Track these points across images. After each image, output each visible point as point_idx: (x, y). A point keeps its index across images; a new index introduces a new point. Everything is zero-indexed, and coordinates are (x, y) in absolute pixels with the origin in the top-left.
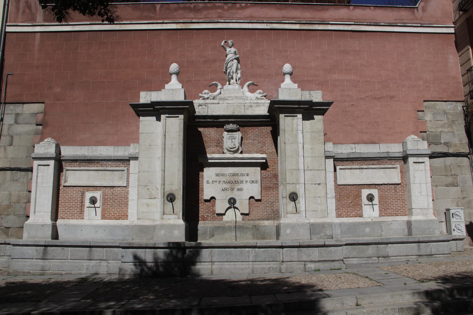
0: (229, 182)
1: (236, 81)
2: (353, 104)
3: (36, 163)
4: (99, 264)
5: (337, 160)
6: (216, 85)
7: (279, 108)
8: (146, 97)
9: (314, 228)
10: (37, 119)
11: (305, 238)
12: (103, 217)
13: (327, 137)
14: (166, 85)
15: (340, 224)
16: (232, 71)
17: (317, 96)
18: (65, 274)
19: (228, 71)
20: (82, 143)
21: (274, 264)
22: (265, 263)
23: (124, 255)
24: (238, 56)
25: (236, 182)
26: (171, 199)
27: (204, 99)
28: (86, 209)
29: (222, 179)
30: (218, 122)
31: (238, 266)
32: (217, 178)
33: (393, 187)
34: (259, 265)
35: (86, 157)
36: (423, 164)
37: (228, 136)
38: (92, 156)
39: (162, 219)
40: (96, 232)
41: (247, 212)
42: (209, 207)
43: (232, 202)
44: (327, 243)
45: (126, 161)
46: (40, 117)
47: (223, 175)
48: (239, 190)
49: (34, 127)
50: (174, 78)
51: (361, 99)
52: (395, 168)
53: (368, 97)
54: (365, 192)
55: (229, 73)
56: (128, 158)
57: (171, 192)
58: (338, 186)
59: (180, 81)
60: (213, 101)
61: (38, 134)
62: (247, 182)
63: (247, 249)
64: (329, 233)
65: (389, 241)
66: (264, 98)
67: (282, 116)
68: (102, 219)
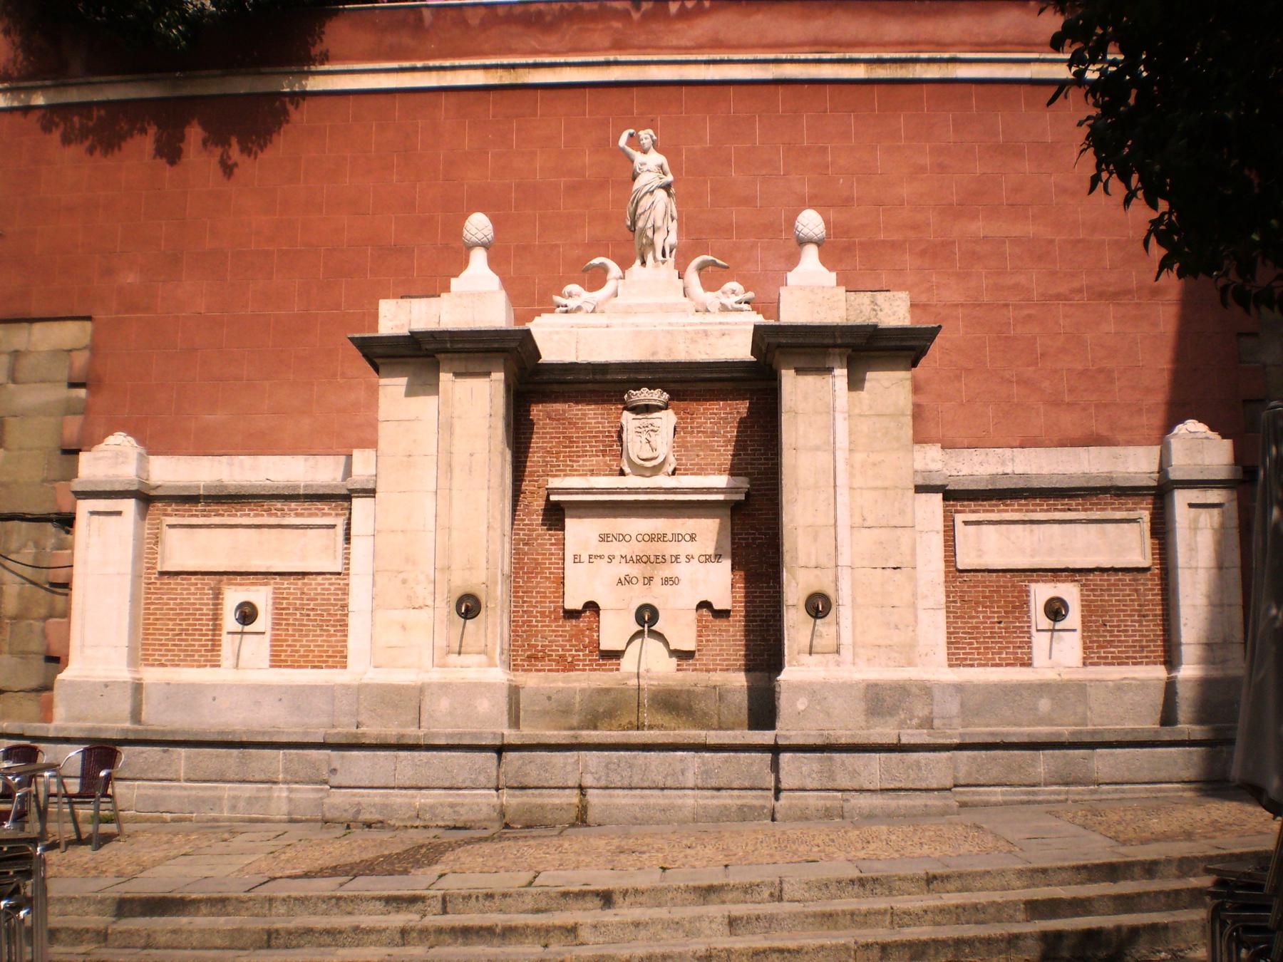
0: (639, 560)
1: (664, 255)
2: (1029, 316)
3: (84, 507)
4: (265, 794)
5: (953, 496)
6: (603, 269)
7: (785, 347)
8: (397, 317)
9: (879, 699)
10: (71, 368)
11: (848, 728)
12: (277, 661)
13: (924, 427)
14: (453, 281)
15: (959, 688)
16: (649, 225)
17: (894, 311)
18: (173, 820)
19: (640, 224)
20: (204, 446)
21: (755, 797)
22: (730, 792)
23: (338, 767)
24: (670, 178)
25: (660, 560)
26: (467, 609)
27: (567, 312)
28: (226, 640)
29: (618, 549)
30: (607, 384)
31: (652, 801)
32: (605, 549)
33: (1128, 577)
34: (713, 797)
35: (226, 487)
36: (1135, 525)
37: (637, 423)
38: (242, 486)
39: (444, 666)
40: (257, 703)
41: (690, 645)
42: (582, 631)
43: (647, 616)
44: (904, 740)
45: (342, 498)
46: (81, 359)
47: (621, 538)
48: (666, 581)
49: (63, 392)
50: (479, 258)
51: (1058, 297)
52: (1134, 521)
53: (1080, 291)
54: (1041, 593)
55: (643, 230)
56: (345, 492)
57: (469, 590)
58: (954, 572)
59: (493, 263)
60: (592, 319)
61: (74, 414)
62: (689, 558)
63: (679, 753)
64: (921, 711)
65: (1098, 739)
66: (746, 306)
67: (743, 407)
68: (272, 666)
